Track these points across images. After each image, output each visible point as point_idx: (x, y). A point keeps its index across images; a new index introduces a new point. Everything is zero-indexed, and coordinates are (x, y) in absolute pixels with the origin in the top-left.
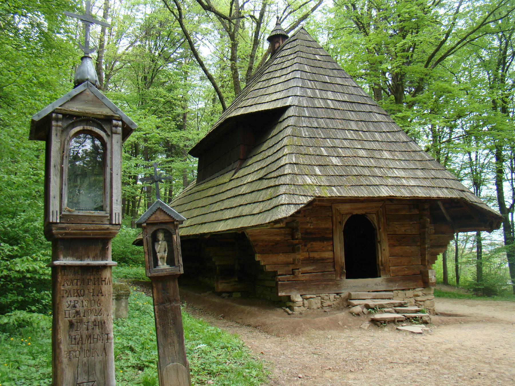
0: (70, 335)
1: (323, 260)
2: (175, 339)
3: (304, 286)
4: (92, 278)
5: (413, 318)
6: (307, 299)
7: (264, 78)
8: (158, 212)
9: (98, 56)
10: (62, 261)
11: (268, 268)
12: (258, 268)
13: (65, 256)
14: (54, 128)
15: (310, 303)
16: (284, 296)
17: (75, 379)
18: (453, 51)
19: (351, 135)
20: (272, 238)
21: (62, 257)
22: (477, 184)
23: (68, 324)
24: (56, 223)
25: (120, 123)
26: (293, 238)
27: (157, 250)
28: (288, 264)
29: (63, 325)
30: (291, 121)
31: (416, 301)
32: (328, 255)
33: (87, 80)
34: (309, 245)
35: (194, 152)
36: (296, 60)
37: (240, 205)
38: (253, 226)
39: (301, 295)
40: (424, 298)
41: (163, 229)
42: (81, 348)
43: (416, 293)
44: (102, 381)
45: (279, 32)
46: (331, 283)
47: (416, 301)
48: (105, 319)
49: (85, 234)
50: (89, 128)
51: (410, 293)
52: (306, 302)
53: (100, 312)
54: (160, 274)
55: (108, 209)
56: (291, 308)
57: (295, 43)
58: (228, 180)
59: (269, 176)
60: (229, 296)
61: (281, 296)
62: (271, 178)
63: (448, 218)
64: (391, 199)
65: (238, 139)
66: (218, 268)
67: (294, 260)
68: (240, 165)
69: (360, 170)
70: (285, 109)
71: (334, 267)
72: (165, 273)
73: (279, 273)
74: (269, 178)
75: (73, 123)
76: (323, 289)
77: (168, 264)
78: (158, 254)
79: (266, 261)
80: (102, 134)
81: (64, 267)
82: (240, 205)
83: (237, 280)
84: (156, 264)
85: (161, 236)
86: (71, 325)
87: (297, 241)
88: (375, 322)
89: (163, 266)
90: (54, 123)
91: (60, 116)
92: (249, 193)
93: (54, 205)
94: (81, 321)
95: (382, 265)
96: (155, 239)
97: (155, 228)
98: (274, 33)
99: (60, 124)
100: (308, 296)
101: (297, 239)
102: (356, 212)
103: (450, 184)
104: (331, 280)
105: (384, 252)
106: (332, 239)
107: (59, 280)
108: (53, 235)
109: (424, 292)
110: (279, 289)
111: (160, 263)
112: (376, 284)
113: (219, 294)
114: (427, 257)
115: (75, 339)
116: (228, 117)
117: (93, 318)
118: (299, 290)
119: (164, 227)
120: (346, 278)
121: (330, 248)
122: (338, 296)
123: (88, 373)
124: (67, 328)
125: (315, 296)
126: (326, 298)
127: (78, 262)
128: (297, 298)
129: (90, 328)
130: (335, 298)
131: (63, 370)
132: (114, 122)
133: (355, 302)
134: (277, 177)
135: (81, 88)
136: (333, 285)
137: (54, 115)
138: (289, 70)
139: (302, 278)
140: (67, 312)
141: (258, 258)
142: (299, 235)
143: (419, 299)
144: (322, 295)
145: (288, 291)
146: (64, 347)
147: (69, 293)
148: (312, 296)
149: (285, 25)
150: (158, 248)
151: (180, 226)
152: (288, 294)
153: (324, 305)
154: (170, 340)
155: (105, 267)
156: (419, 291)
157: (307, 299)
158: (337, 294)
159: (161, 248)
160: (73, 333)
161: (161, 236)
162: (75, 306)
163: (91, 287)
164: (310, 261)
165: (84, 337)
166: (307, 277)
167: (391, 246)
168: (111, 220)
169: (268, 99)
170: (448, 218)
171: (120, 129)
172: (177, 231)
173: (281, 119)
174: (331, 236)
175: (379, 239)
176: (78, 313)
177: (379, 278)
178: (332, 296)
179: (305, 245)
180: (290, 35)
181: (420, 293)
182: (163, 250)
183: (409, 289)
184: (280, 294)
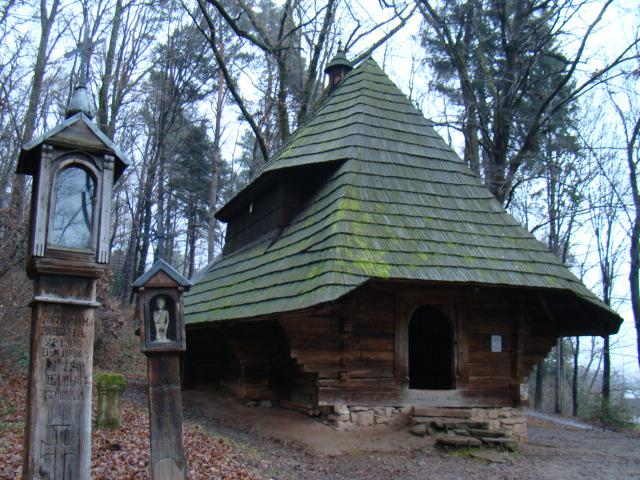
0: (46, 375)
1: (380, 363)
2: (172, 430)
3: (353, 395)
4: (74, 317)
5: (492, 442)
6: (356, 412)
7: (317, 121)
8: (160, 276)
9: (104, 85)
10: (44, 297)
11: (306, 369)
13: (47, 292)
14: (43, 160)
15: (359, 417)
16: (326, 406)
17: (49, 420)
19: (426, 201)
21: (43, 293)
22: (607, 280)
23: (45, 363)
24: (40, 257)
25: (113, 158)
26: (342, 331)
27: (156, 320)
28: (333, 365)
29: (40, 362)
30: (347, 179)
31: (502, 424)
32: (386, 356)
33: (80, 111)
34: (362, 343)
35: (221, 216)
36: (359, 100)
37: (276, 285)
38: (288, 312)
39: (348, 407)
40: (512, 421)
41: (163, 295)
42: (58, 390)
43: (502, 413)
44: (77, 427)
45: (341, 62)
46: (389, 393)
47: (502, 424)
48: (84, 360)
49: (70, 271)
51: (494, 413)
52: (354, 415)
53: (79, 354)
54: (158, 349)
55: (95, 247)
56: (332, 423)
57: (359, 77)
58: (262, 253)
59: (313, 249)
60: (256, 405)
61: (322, 407)
62: (316, 251)
64: (471, 285)
65: (279, 198)
66: (243, 367)
67: (341, 360)
68: (280, 233)
69: (433, 247)
70: (340, 162)
71: (394, 373)
72: (162, 348)
73: (321, 376)
74: (316, 254)
75: (63, 156)
76: (378, 400)
77: (168, 337)
78: (157, 325)
79: (306, 360)
80: (93, 167)
81: (46, 303)
82: (276, 285)
83: (267, 383)
84: (154, 338)
85: (161, 303)
86: (49, 364)
88: (441, 445)
89: (162, 339)
90: (44, 155)
91: (51, 147)
92: (287, 270)
94: (59, 361)
96: (154, 307)
97: (154, 293)
98: (336, 63)
99: (50, 155)
100: (357, 408)
101: (348, 332)
103: (553, 270)
104: (389, 389)
107: (40, 316)
108: (36, 269)
110: (320, 397)
111: (158, 336)
112: (449, 398)
113: (243, 401)
114: (520, 366)
115: (52, 378)
116: (266, 170)
117: (72, 359)
118: (346, 399)
119: (166, 292)
120: (410, 388)
121: (389, 347)
122: (397, 411)
123: (63, 416)
124: (45, 367)
125: (366, 409)
126: (381, 412)
127: (59, 300)
128: (343, 409)
129: (68, 369)
130: (393, 413)
131: (37, 410)
132: (107, 157)
133: (419, 420)
134: (324, 250)
135: (73, 119)
136: (391, 396)
137: (44, 146)
138: (350, 112)
139: (350, 383)
140: (45, 350)
142: (348, 328)
143: (505, 421)
144: (376, 408)
145: (331, 399)
146: (39, 386)
147: (48, 331)
148: (362, 408)
149: (350, 57)
150: (157, 317)
151: (185, 294)
152: (331, 404)
153: (378, 421)
154: (164, 430)
155: (88, 307)
156: (506, 411)
157: (356, 412)
158: (397, 408)
160: (50, 373)
161: (161, 303)
162: (53, 345)
163: (72, 327)
164: (367, 363)
165: (62, 378)
166: (357, 383)
167: (472, 350)
168: (97, 258)
169: (319, 148)
171: (112, 165)
172: (181, 298)
173: (335, 177)
174: (391, 331)
175: (456, 339)
176: (56, 352)
177: (453, 391)
178: (389, 410)
179: (358, 342)
180: (355, 67)
181: (508, 414)
182: (163, 320)
183: (493, 408)
184: (320, 403)
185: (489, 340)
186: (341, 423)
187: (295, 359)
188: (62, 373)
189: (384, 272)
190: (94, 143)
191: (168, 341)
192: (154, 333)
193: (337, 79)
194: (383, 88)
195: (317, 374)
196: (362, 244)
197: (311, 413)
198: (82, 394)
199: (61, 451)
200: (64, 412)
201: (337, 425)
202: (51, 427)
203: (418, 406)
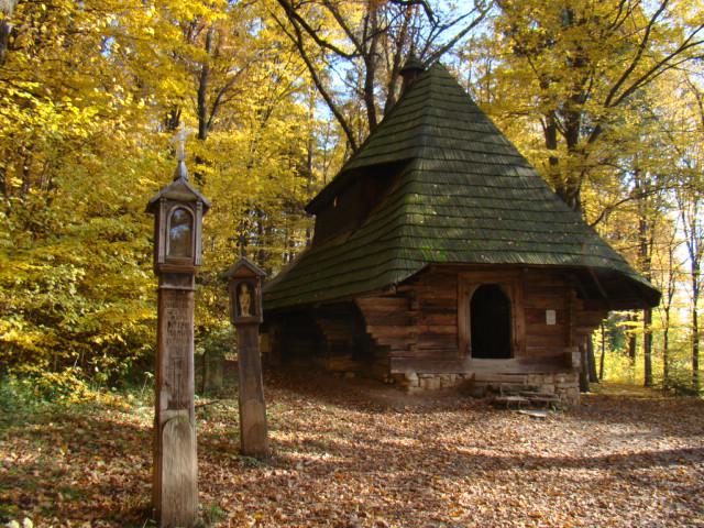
1: (444, 335)
10: (166, 286)
11: (381, 342)
12: (371, 340)
13: (167, 283)
18: (626, 86)
20: (386, 309)
32: (450, 329)
39: (418, 374)
50: (182, 206)
52: (422, 381)
56: (404, 389)
63: (604, 294)
72: (245, 321)
73: (393, 348)
81: (166, 290)
84: (240, 313)
85: (244, 289)
86: (169, 324)
87: (413, 313)
89: (245, 314)
93: (161, 254)
94: (175, 323)
95: (516, 344)
100: (425, 375)
102: (486, 282)
105: (520, 328)
106: (456, 312)
109: (568, 378)
112: (507, 366)
120: (473, 356)
123: (178, 353)
126: (446, 378)
141: (369, 329)
142: (416, 305)
155: (190, 291)
158: (461, 375)
159: (245, 299)
161: (244, 289)
167: (529, 323)
170: (604, 294)
171: (201, 208)
174: (455, 308)
176: (173, 317)
177: (511, 360)
178: (453, 377)
179: (425, 318)
184: (393, 371)
185: (545, 314)
186: (411, 388)
187: (370, 334)
188: (177, 330)
189: (440, 257)
190: (189, 196)
191: (248, 315)
192: (239, 309)
193: (410, 81)
194: (450, 90)
195: (389, 346)
196: (424, 234)
197: (386, 380)
198: (188, 341)
199: (177, 373)
200: (179, 351)
201: (407, 390)
202: (171, 358)
203: (479, 373)
